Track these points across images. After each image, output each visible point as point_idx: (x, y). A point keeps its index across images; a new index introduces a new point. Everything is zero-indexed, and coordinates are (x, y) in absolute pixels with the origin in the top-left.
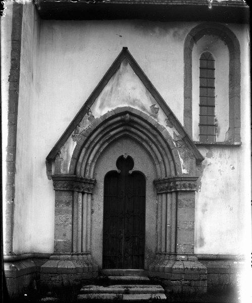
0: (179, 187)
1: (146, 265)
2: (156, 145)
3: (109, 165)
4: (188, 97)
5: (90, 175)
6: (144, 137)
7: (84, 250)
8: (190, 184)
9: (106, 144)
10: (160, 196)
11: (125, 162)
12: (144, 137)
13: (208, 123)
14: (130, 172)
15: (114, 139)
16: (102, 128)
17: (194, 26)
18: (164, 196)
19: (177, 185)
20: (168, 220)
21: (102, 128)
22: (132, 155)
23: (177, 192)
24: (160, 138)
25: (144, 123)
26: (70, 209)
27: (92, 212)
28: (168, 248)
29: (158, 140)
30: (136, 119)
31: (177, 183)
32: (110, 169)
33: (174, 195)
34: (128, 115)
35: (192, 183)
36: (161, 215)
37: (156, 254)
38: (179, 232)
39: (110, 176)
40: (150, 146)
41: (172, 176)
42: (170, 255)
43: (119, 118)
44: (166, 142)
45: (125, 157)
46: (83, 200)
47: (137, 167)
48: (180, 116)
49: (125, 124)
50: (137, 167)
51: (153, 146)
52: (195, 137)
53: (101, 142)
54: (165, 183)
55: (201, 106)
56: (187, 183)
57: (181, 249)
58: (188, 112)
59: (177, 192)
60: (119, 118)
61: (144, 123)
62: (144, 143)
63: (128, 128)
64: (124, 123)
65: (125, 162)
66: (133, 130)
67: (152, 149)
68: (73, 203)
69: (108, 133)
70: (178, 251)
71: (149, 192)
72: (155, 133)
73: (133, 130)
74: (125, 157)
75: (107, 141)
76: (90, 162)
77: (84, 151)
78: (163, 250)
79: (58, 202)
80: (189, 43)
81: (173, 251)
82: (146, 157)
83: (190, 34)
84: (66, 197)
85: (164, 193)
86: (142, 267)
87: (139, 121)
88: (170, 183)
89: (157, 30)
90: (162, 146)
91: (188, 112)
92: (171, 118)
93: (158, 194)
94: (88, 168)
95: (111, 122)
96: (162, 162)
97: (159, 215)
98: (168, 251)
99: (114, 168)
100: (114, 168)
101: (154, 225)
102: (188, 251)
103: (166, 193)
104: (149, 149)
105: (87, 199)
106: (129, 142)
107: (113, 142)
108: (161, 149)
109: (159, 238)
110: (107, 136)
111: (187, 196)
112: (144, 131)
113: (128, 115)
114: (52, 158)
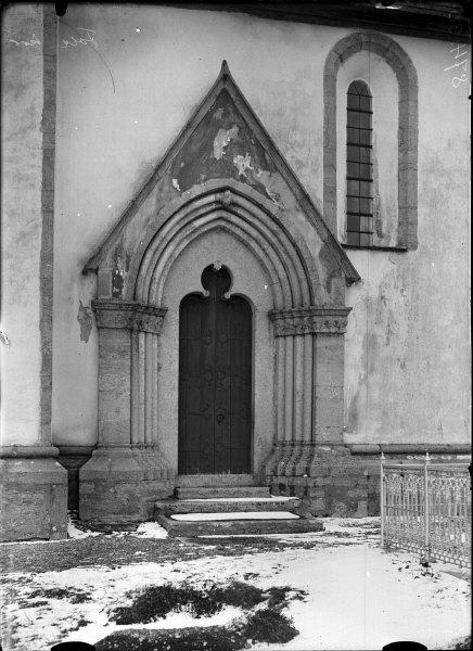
2: (275, 250)
4: (330, 166)
6: (254, 233)
7: (149, 440)
11: (217, 277)
12: (254, 233)
13: (360, 207)
14: (228, 296)
15: (199, 233)
18: (289, 339)
20: (299, 382)
22: (230, 265)
23: (314, 335)
24: (283, 237)
27: (159, 368)
28: (298, 430)
33: (309, 338)
36: (285, 376)
38: (318, 403)
39: (190, 302)
42: (284, 445)
44: (294, 245)
47: (238, 287)
48: (317, 193)
50: (238, 287)
51: (270, 250)
52: (340, 240)
53: (177, 239)
55: (349, 179)
56: (332, 319)
57: (322, 435)
58: (330, 191)
60: (212, 198)
62: (253, 244)
63: (224, 214)
65: (217, 277)
66: (234, 219)
70: (318, 439)
71: (261, 331)
72: (275, 227)
74: (218, 267)
76: (157, 275)
78: (288, 438)
80: (332, 66)
81: (307, 438)
83: (335, 50)
84: (120, 340)
86: (184, 468)
89: (240, 14)
91: (330, 191)
92: (305, 200)
93: (277, 337)
96: (286, 280)
97: (280, 374)
98: (298, 438)
100: (198, 287)
101: (270, 394)
102: (333, 439)
105: (153, 341)
107: (199, 237)
108: (284, 256)
109: (280, 416)
110: (188, 227)
111: (333, 341)
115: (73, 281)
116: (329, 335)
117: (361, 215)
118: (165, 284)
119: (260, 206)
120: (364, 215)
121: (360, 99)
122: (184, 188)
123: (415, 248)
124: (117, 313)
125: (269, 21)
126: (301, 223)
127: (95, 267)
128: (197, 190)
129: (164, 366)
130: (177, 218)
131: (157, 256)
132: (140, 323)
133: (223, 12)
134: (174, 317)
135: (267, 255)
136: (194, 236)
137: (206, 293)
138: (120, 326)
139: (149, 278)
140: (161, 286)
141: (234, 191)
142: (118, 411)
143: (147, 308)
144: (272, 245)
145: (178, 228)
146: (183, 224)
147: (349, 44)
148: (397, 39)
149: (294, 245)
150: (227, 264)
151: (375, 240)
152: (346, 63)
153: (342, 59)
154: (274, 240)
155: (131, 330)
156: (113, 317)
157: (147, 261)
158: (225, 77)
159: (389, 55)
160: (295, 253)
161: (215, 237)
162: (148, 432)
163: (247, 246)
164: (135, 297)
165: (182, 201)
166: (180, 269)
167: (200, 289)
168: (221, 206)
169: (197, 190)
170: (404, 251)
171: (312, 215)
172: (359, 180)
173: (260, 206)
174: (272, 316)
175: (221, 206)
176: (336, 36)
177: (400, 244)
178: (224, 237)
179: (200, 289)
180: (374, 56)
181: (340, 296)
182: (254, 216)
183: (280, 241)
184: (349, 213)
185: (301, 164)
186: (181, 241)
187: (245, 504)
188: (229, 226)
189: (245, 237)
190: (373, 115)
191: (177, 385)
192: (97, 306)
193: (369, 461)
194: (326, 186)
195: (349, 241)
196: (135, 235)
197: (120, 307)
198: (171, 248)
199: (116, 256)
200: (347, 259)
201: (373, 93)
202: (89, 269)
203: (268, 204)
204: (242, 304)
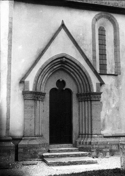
0: (92, 98)
1: (74, 139)
3: (53, 85)
5: (42, 90)
6: (72, 70)
8: (98, 97)
9: (51, 73)
10: (81, 103)
11: (60, 83)
12: (72, 70)
14: (64, 89)
16: (50, 65)
17: (97, 13)
18: (83, 102)
19: (91, 97)
21: (50, 65)
22: (65, 79)
24: (81, 71)
25: (72, 63)
26: (34, 110)
29: (80, 72)
30: (68, 61)
31: (91, 96)
32: (53, 87)
33: (89, 102)
34: (64, 58)
35: (99, 96)
37: (79, 135)
39: (53, 91)
40: (75, 75)
41: (88, 92)
43: (59, 60)
45: (61, 80)
46: (39, 104)
49: (62, 64)
52: (98, 70)
53: (49, 72)
54: (84, 96)
56: (96, 96)
59: (91, 101)
60: (59, 60)
61: (72, 63)
64: (62, 62)
66: (66, 66)
67: (76, 77)
68: (36, 105)
69: (53, 67)
70: (93, 133)
73: (66, 66)
74: (61, 80)
75: (51, 72)
77: (40, 77)
78: (84, 132)
79: (25, 107)
80: (94, 22)
81: (90, 132)
82: (72, 81)
83: (95, 17)
84: (31, 103)
85: (83, 101)
87: (70, 62)
88: (87, 95)
90: (82, 76)
91: (94, 57)
92: (87, 60)
93: (79, 101)
94: (42, 86)
95: (55, 62)
99: (55, 86)
100: (55, 86)
103: (85, 101)
104: (74, 76)
106: (62, 72)
111: (97, 102)
112: (73, 67)
113: (64, 58)
114: (22, 82)
116: (96, 100)
132: (37, 98)
134: (48, 96)
147: (99, 16)
148: (112, 14)
150: (64, 79)
153: (97, 20)
161: (60, 71)
170: (117, 75)
177: (115, 73)
180: (106, 19)
201: (105, 29)
204: (69, 91)
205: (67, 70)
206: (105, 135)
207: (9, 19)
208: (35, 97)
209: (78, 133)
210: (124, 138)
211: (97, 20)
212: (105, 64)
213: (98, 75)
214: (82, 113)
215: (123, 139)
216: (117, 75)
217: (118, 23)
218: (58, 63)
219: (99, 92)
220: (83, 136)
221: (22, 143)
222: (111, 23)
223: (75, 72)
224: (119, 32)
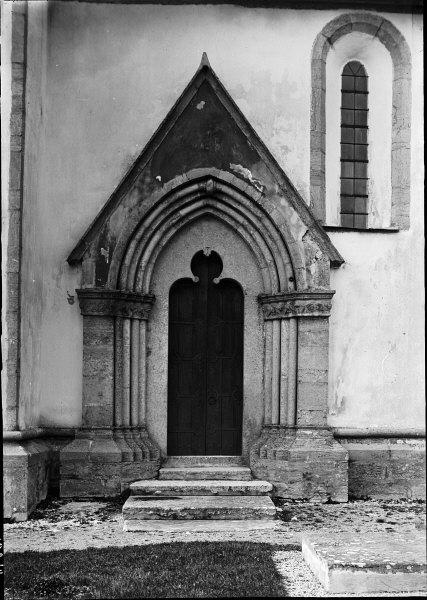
4: (319, 148)
5: (144, 287)
7: (135, 422)
10: (268, 325)
11: (206, 263)
14: (217, 281)
22: (220, 251)
23: (297, 319)
24: (267, 223)
30: (225, 189)
35: (323, 303)
39: (179, 288)
43: (195, 187)
45: (207, 253)
47: (228, 272)
50: (228, 272)
51: (256, 236)
53: (164, 228)
58: (318, 176)
60: (195, 187)
63: (211, 202)
65: (206, 263)
66: (219, 206)
68: (117, 336)
73: (219, 206)
74: (207, 253)
76: (143, 264)
78: (274, 421)
80: (320, 50)
83: (323, 33)
84: (103, 328)
87: (230, 192)
91: (318, 176)
93: (265, 320)
107: (186, 226)
111: (317, 325)
115: (61, 273)
116: (312, 318)
117: (356, 196)
118: (153, 272)
119: (243, 194)
120: (360, 196)
121: (355, 82)
122: (165, 180)
123: (407, 227)
124: (109, 304)
125: (271, 10)
126: (283, 207)
127: (79, 259)
128: (179, 180)
129: (153, 351)
130: (161, 208)
131: (143, 245)
132: (124, 310)
133: (208, 5)
134: (164, 303)
135: (254, 240)
136: (181, 225)
137: (217, 281)
138: (102, 313)
139: (134, 266)
140: (149, 274)
141: (216, 180)
142: (101, 395)
143: (130, 295)
144: (257, 230)
145: (163, 217)
146: (168, 213)
147: (338, 26)
148: (388, 16)
149: (278, 230)
150: (216, 250)
151: (371, 223)
152: (336, 45)
153: (330, 41)
154: (258, 225)
155: (114, 318)
156: (95, 306)
157: (131, 251)
158: (205, 71)
159: (381, 34)
160: (279, 238)
161: (205, 225)
162: (135, 415)
163: (236, 231)
164: (118, 284)
165: (164, 191)
166: (170, 254)
167: (189, 274)
168: (204, 194)
169: (179, 180)
170: (396, 231)
171: (294, 199)
172: (354, 161)
173: (243, 194)
174: (261, 300)
175: (204, 194)
176: (320, 21)
177: (392, 225)
178: (213, 225)
179: (189, 274)
180: (366, 36)
181: (323, 278)
182: (240, 203)
183: (264, 226)
184: (343, 195)
185: (286, 149)
186: (168, 230)
187: (164, 490)
188: (216, 213)
189: (232, 223)
190: (369, 95)
191: (166, 368)
192: (83, 297)
193: (356, 445)
194: (313, 171)
195: (342, 223)
196: (120, 223)
197: (102, 295)
198: (156, 238)
199: (101, 244)
200: (329, 241)
201: (368, 72)
202: (74, 260)
203: (250, 191)
204: (233, 288)
205: (226, 219)
206: (342, 432)
207: (13, 68)
208: (113, 307)
209: (259, 422)
210: (424, 442)
211: (331, 43)
212: (362, 193)
213: (321, 230)
214: (139, 370)
215: (420, 446)
216: (396, 231)
217: (407, 47)
218: (193, 198)
219: (325, 289)
220: (271, 431)
221: (71, 448)
222: (377, 42)
223: (250, 227)
224: (409, 79)
